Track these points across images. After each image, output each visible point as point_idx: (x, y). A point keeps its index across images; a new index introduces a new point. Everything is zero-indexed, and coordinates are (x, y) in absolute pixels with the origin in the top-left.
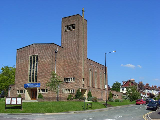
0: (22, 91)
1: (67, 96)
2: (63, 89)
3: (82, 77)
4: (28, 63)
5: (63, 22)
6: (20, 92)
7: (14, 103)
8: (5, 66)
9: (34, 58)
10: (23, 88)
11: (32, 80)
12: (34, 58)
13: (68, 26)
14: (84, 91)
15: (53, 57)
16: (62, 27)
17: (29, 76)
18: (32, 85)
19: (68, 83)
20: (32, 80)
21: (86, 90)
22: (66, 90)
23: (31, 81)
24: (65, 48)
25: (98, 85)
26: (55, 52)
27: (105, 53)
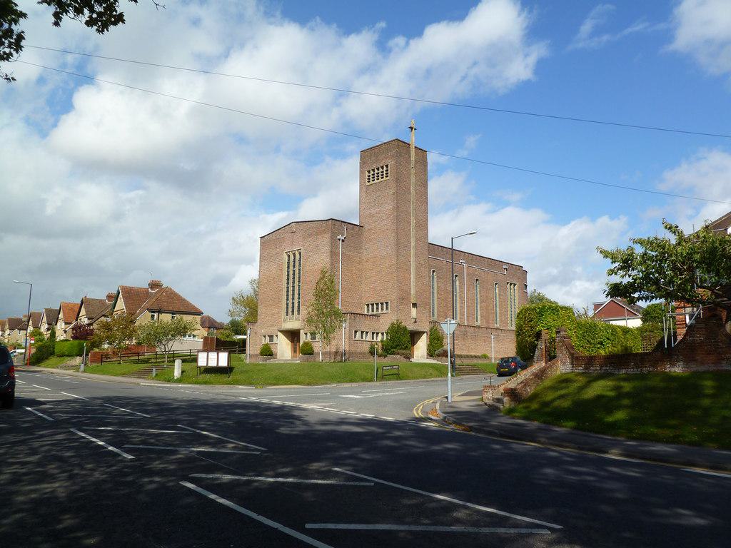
0: (271, 337)
1: (366, 348)
2: (356, 332)
3: (408, 299)
4: (282, 270)
5: (363, 163)
6: (268, 338)
7: (213, 363)
8: (610, 247)
9: (294, 255)
10: (425, 327)
11: (290, 310)
12: (294, 255)
13: (374, 170)
14: (415, 336)
15: (334, 254)
16: (362, 172)
17: (284, 302)
18: (292, 324)
19: (372, 315)
20: (290, 310)
21: (424, 332)
22: (367, 333)
23: (385, 309)
24: (367, 227)
25: (486, 318)
26: (339, 239)
27: (452, 239)
